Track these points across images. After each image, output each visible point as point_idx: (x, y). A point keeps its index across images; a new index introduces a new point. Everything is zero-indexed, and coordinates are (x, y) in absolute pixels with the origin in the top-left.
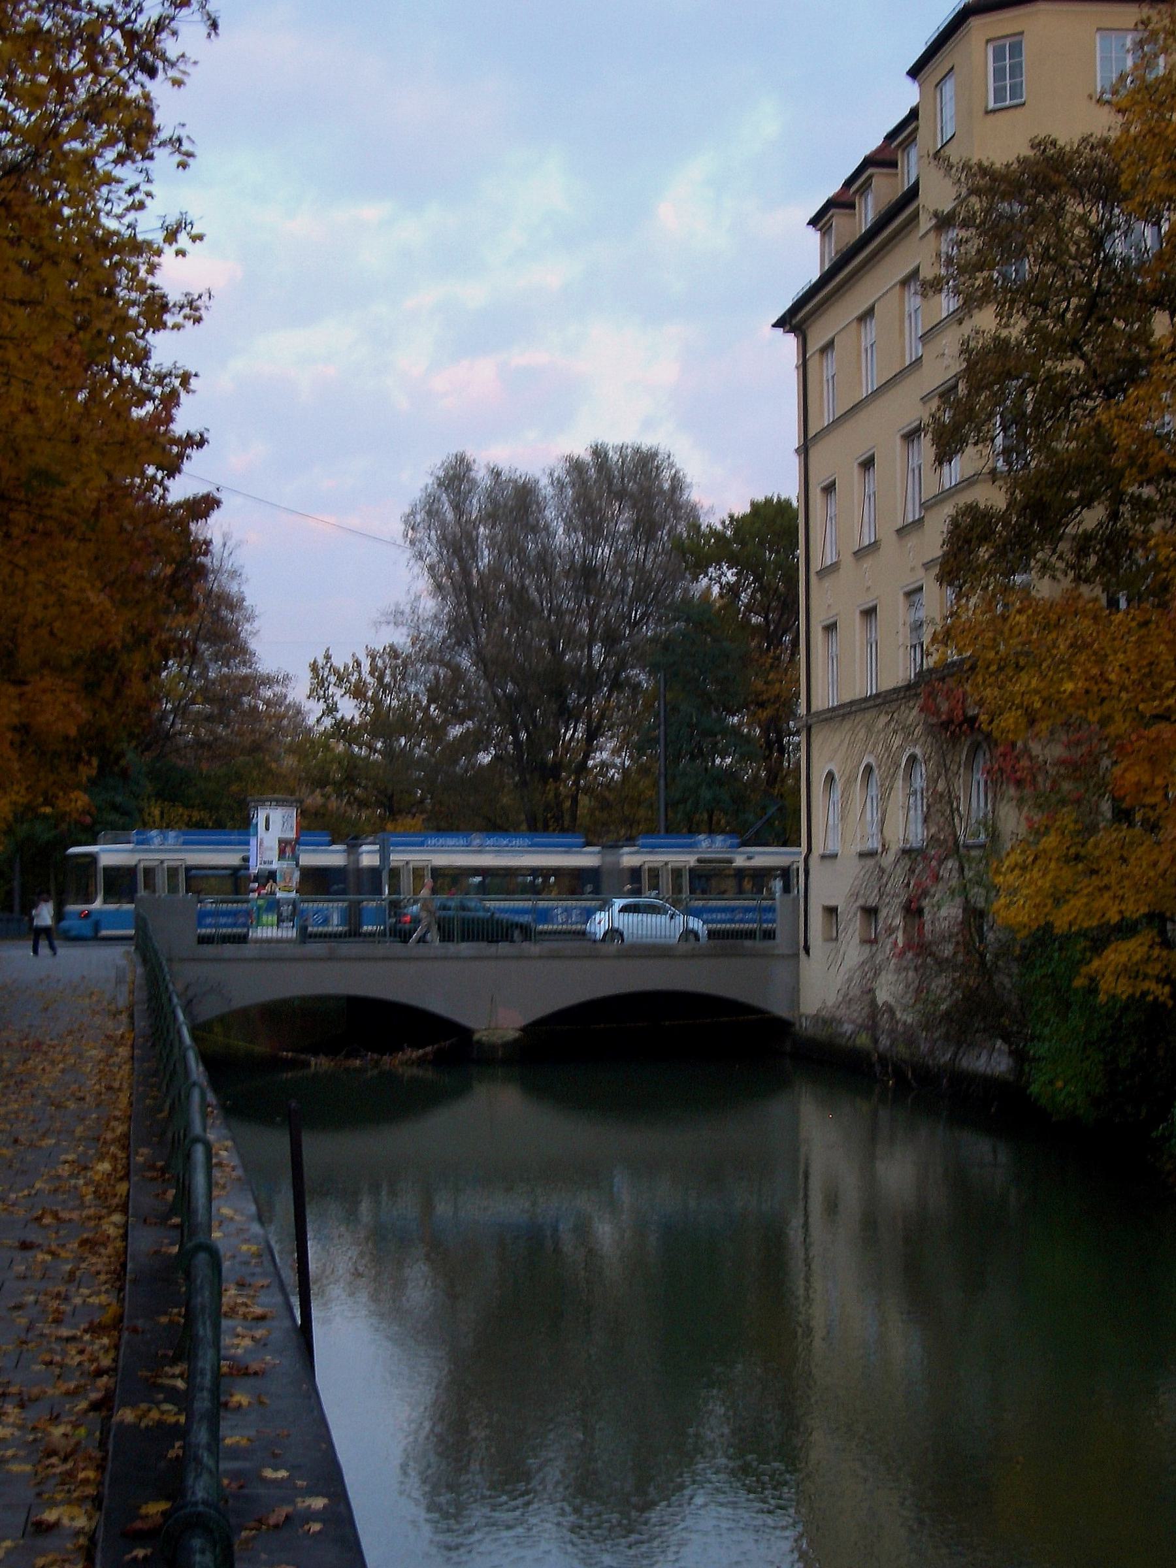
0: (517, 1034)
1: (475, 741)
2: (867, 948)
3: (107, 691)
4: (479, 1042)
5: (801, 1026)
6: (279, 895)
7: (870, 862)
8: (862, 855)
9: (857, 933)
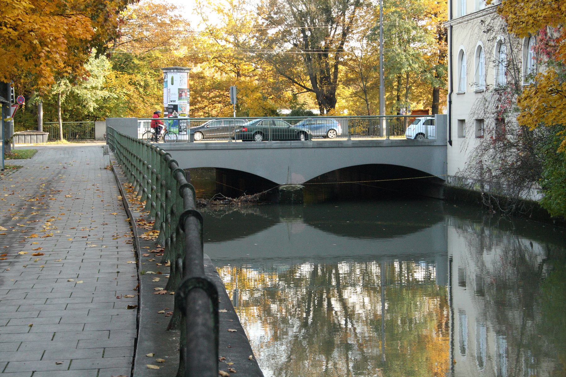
2: (479, 139)
3: (101, 19)
4: (282, 190)
5: (448, 182)
7: (480, 96)
8: (477, 92)
9: (474, 133)
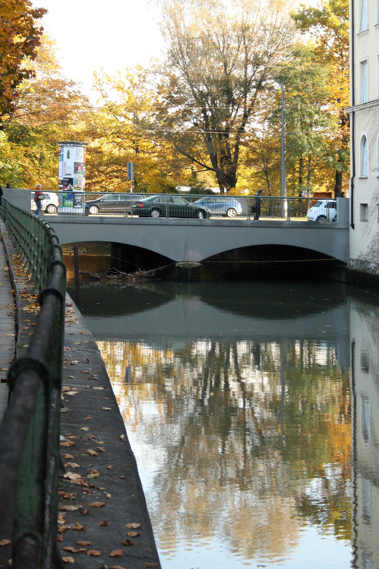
0: (199, 264)
1: (185, 115)
4: (179, 267)
6: (74, 191)
